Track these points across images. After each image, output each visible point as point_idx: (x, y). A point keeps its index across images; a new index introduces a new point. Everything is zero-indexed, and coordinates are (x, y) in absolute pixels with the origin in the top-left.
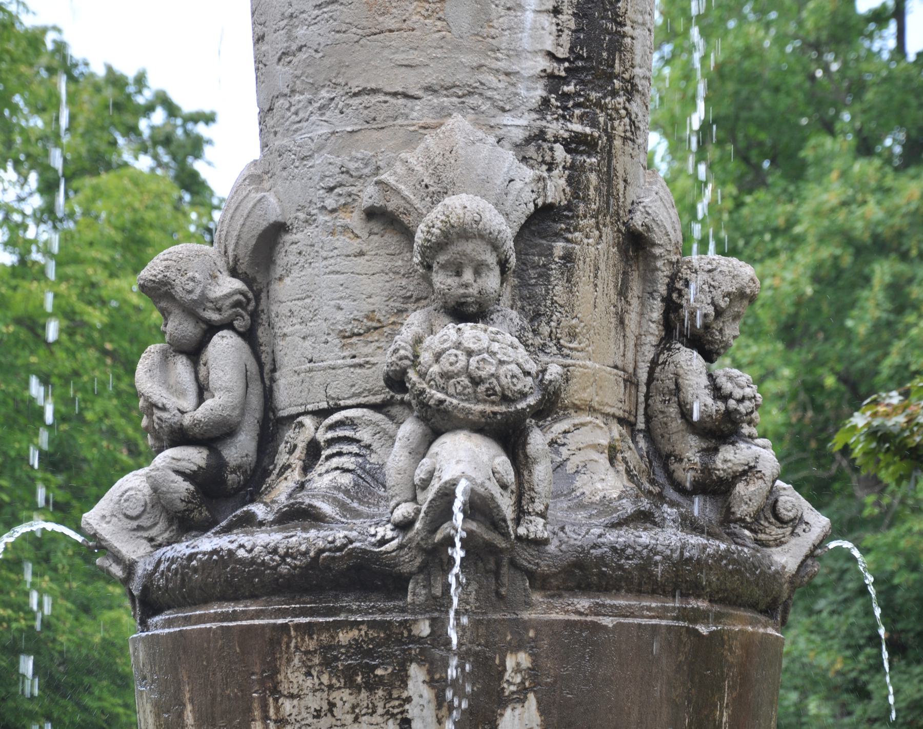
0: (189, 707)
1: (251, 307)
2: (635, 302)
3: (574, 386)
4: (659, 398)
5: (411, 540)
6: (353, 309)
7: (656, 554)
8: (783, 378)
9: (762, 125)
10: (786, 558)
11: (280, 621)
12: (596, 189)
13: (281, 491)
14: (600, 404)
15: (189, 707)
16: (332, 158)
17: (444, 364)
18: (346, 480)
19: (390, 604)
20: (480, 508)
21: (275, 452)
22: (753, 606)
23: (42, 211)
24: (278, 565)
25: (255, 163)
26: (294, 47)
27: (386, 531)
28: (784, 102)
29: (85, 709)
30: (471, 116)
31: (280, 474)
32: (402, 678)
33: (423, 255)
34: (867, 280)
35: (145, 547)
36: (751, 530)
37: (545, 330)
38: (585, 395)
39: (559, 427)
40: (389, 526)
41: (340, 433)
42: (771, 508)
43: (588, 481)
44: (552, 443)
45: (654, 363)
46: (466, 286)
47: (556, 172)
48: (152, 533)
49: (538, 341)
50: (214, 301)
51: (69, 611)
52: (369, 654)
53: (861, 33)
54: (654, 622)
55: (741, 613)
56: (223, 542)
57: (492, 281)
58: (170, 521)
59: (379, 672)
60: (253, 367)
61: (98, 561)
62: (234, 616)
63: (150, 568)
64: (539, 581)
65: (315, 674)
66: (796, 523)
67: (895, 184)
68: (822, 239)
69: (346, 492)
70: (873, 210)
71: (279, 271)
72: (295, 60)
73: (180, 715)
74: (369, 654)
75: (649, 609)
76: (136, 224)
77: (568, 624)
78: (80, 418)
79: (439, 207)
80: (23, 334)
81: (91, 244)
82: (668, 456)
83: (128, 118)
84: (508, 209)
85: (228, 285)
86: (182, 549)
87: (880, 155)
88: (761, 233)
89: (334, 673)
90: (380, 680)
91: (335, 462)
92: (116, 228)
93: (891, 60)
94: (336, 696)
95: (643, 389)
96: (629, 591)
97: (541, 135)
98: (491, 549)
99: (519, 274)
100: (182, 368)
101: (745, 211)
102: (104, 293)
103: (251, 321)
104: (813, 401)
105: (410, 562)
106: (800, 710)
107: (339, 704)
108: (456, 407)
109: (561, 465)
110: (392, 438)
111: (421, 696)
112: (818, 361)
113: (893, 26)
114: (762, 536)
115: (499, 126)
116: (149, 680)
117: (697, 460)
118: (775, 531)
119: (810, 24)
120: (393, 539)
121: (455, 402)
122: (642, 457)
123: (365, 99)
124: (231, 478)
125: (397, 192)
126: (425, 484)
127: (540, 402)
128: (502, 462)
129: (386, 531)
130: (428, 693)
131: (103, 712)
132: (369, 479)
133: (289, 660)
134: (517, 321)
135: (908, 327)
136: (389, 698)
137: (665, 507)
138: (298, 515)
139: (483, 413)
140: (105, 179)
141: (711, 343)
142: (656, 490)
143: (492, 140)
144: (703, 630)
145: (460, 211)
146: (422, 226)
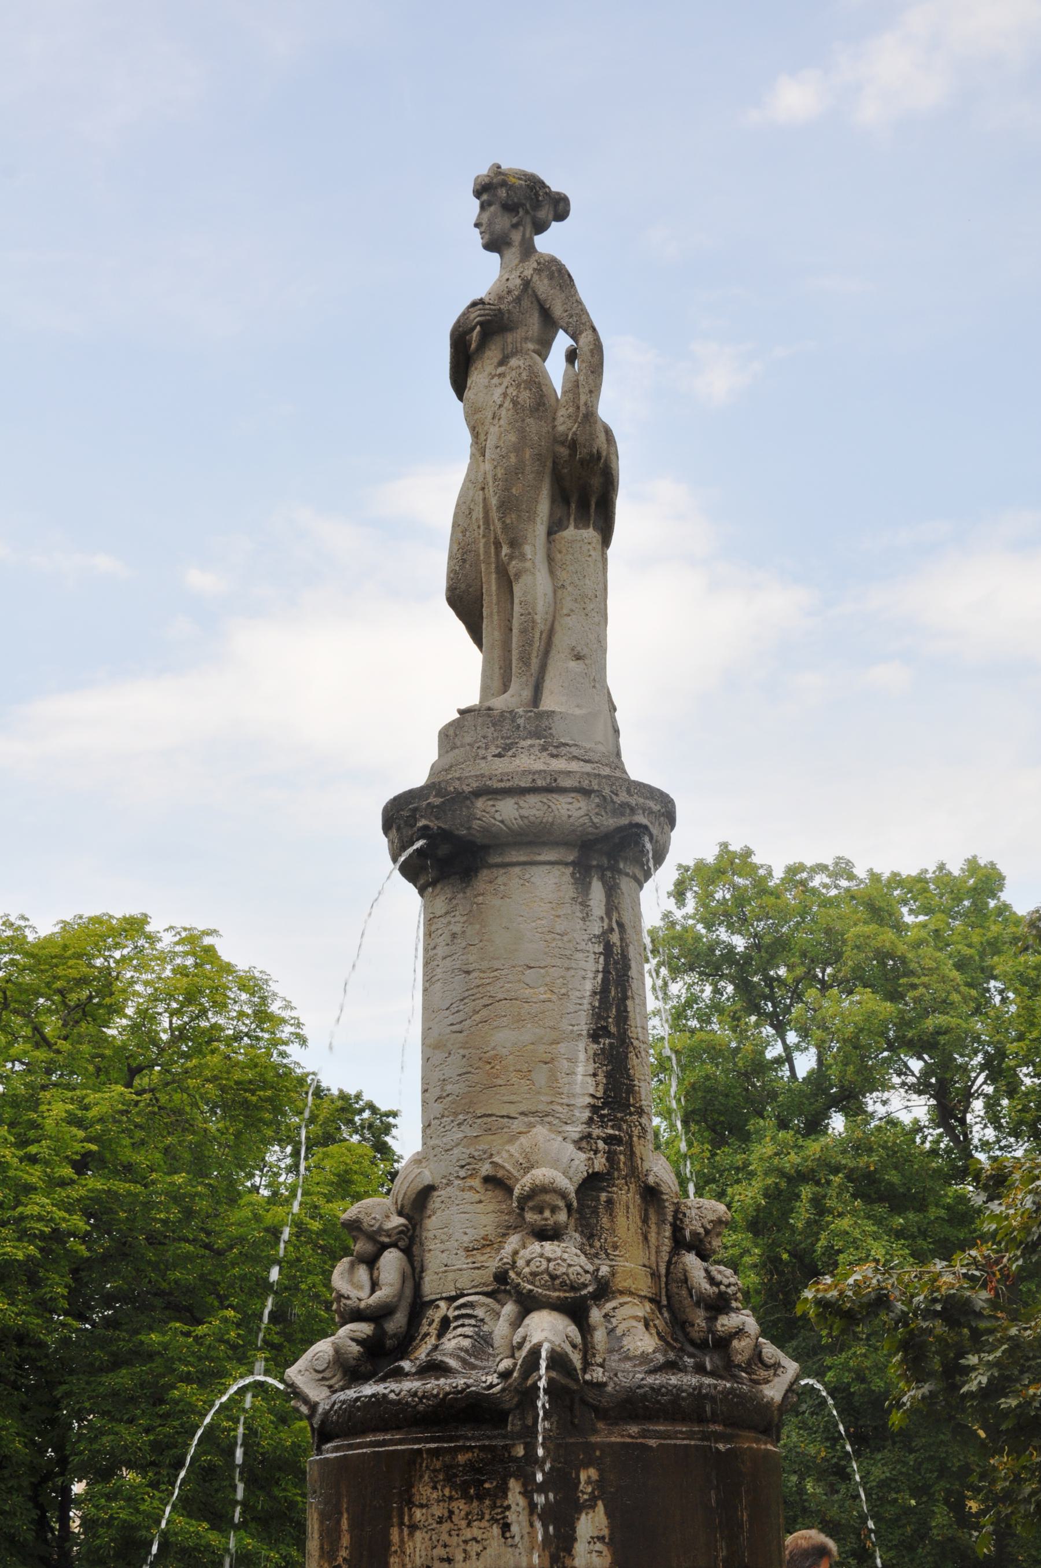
0: (345, 1516)
1: (409, 1234)
2: (653, 1227)
3: (618, 1278)
4: (675, 1285)
5: (510, 1385)
6: (474, 1234)
7: (683, 1391)
8: (755, 1254)
9: (720, 1114)
10: (774, 1392)
11: (416, 1447)
12: (624, 1163)
13: (422, 1353)
14: (636, 1289)
15: (345, 1516)
16: (464, 1150)
17: (533, 1267)
18: (466, 1343)
19: (496, 1432)
20: (558, 1360)
21: (420, 1324)
22: (754, 1428)
23: (291, 1166)
24: (417, 1405)
25: (418, 1153)
26: (445, 1094)
27: (493, 1379)
28: (732, 1102)
29: (275, 1498)
30: (548, 1126)
31: (422, 1339)
32: (504, 1491)
33: (519, 1202)
34: (798, 1196)
35: (326, 1392)
36: (747, 1373)
37: (597, 1244)
38: (626, 1284)
39: (609, 1305)
40: (496, 1375)
41: (463, 1311)
42: (757, 1355)
43: (632, 1339)
44: (606, 1316)
45: (669, 1263)
46: (546, 1219)
47: (599, 1155)
48: (332, 1382)
49: (593, 1251)
50: (387, 1231)
51: (272, 1422)
52: (479, 1471)
53: (771, 1069)
54: (685, 1442)
55: (746, 1433)
56: (379, 1388)
57: (562, 1217)
58: (345, 1374)
59: (487, 1485)
60: (408, 1270)
61: (293, 1403)
62: (384, 1443)
63: (327, 1407)
64: (602, 1414)
65: (439, 1487)
66: (777, 1366)
67: (803, 1144)
68: (766, 1174)
69: (466, 1351)
70: (794, 1158)
71: (429, 1212)
72: (445, 1101)
73: (338, 1522)
74: (479, 1471)
75: (681, 1432)
76: (346, 1171)
77: (624, 1445)
78: (297, 1289)
79: (529, 1175)
80: (269, 1237)
81: (318, 1184)
82: (685, 1322)
83: (349, 1116)
84: (571, 1175)
85: (397, 1221)
86: (351, 1393)
87: (792, 1129)
88: (729, 1170)
89: (453, 1487)
90: (487, 1493)
91: (460, 1331)
92: (334, 1175)
93: (789, 1082)
94: (454, 1504)
95: (664, 1279)
96: (666, 1419)
97: (589, 1136)
98: (566, 1389)
99: (580, 1211)
100: (362, 1273)
101: (718, 1158)
102: (322, 1211)
103: (410, 1242)
104: (776, 1268)
105: (510, 1401)
106: (801, 1490)
107: (457, 1511)
108: (540, 1294)
109: (613, 1330)
110: (498, 1315)
111: (518, 1505)
112: (775, 1244)
113: (787, 1065)
114: (755, 1377)
115: (564, 1132)
116: (318, 1494)
117: (704, 1325)
118: (763, 1373)
119: (740, 1064)
120: (498, 1384)
121: (540, 1291)
122: (666, 1323)
123: (485, 1119)
124: (389, 1343)
125: (503, 1167)
126: (520, 1346)
127: (595, 1290)
128: (573, 1330)
129: (493, 1379)
130: (522, 1502)
131: (286, 1501)
132: (482, 1342)
133: (421, 1477)
134: (579, 1239)
135: (829, 1223)
136: (494, 1507)
137: (686, 1359)
138: (434, 1368)
139: (558, 1298)
140: (333, 1148)
141: (705, 1250)
142: (678, 1345)
143: (560, 1139)
144: (721, 1447)
145: (541, 1177)
146: (518, 1186)
